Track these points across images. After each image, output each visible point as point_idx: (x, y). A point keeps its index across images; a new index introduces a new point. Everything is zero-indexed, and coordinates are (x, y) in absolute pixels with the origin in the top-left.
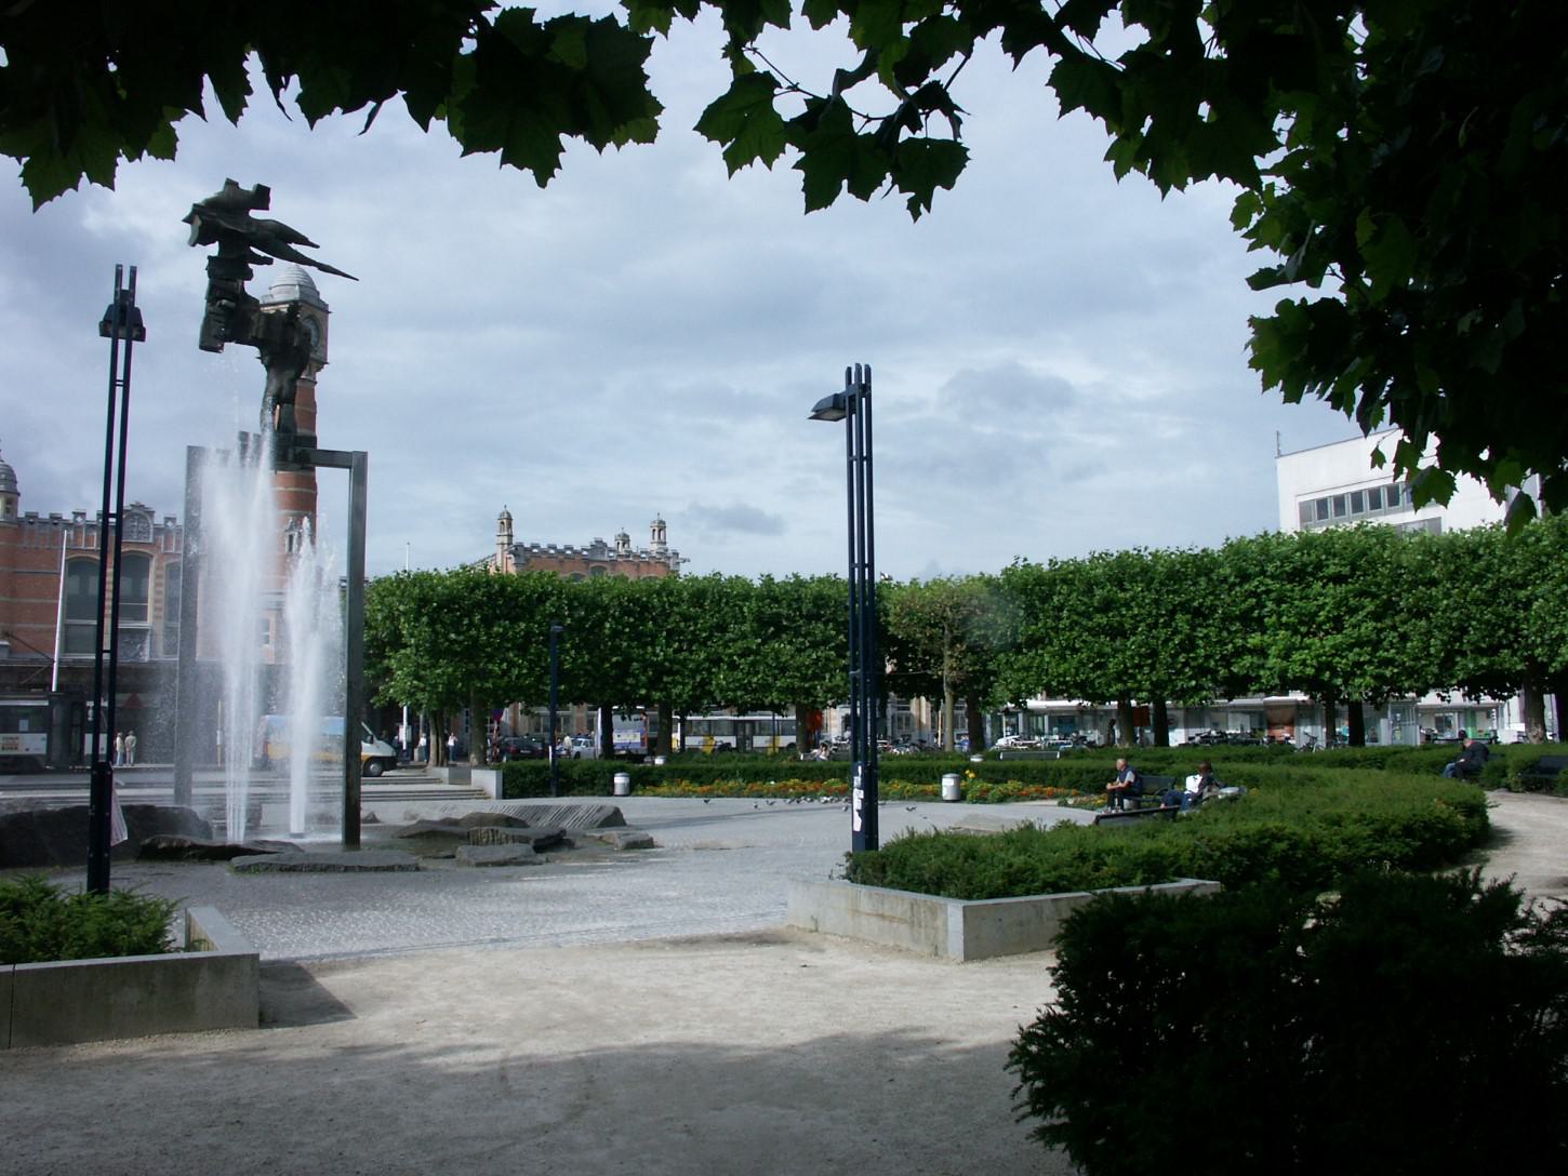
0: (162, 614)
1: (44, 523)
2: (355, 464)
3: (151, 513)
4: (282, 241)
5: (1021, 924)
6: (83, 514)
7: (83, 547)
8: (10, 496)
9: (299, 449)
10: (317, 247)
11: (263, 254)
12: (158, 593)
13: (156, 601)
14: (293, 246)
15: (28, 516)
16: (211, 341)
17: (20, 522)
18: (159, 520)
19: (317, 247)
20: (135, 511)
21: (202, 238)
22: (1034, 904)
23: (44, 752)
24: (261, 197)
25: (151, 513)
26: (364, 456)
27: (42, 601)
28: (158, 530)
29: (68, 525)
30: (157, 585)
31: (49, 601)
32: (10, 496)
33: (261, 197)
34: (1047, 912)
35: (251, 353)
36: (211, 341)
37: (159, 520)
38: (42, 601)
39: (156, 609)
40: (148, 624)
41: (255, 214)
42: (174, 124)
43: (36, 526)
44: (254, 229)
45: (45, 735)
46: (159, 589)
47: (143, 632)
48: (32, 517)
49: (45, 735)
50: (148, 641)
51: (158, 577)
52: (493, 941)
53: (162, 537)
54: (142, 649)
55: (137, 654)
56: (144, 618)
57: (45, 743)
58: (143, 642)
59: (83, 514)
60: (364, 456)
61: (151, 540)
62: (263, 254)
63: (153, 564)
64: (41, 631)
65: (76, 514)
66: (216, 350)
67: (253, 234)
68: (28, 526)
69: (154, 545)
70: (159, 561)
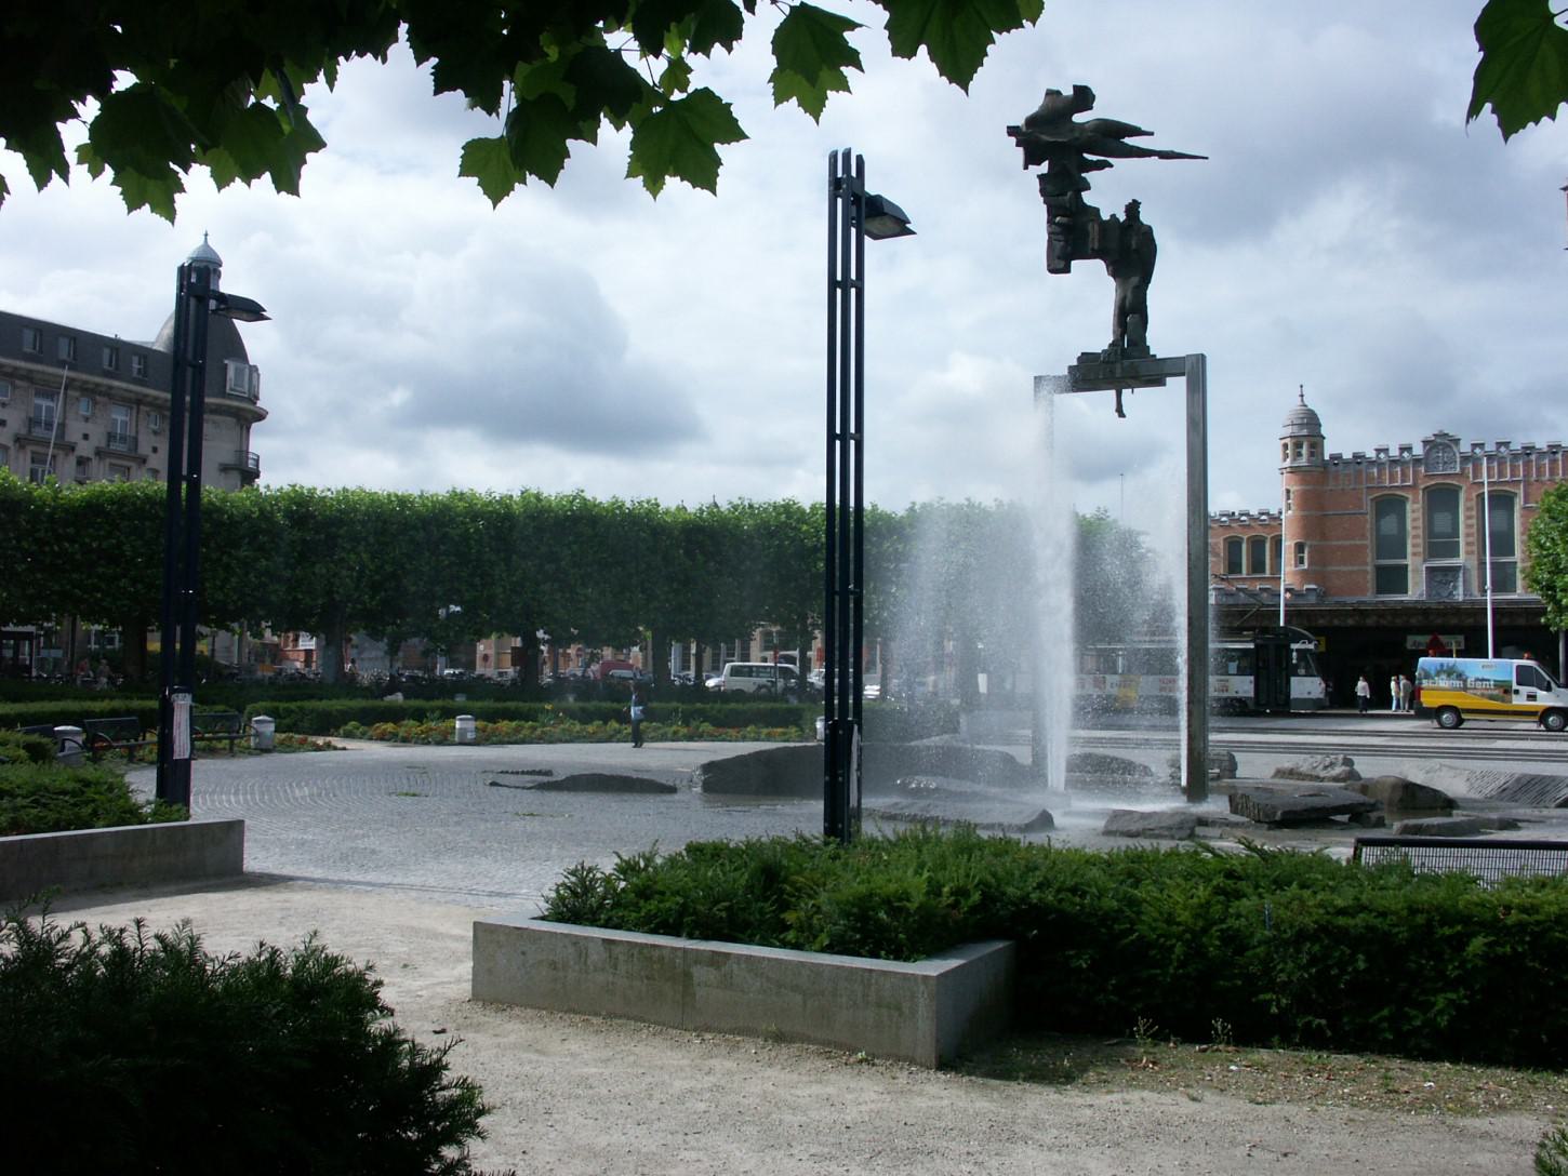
0: (1421, 550)
1: (1347, 463)
2: (1193, 370)
3: (1457, 441)
4: (1114, 139)
5: (553, 965)
6: (1386, 450)
7: (1387, 484)
8: (1313, 439)
9: (1126, 362)
10: (1152, 134)
11: (1095, 158)
12: (1469, 526)
13: (1468, 535)
14: (1127, 140)
15: (1333, 457)
16: (1059, 262)
17: (1325, 464)
18: (1465, 448)
19: (1152, 134)
20: (1439, 440)
21: (1031, 159)
22: (576, 941)
23: (1252, 694)
24: (1083, 97)
25: (1457, 441)
26: (1201, 359)
27: (1352, 542)
28: (1465, 459)
29: (1372, 463)
30: (1468, 518)
31: (1358, 542)
32: (1313, 439)
33: (1083, 97)
34: (594, 957)
35: (1099, 265)
36: (1059, 262)
37: (1465, 448)
38: (1352, 542)
39: (1468, 544)
40: (1460, 561)
41: (1078, 118)
42: (59, 125)
43: (1341, 467)
44: (1077, 134)
45: (1252, 678)
46: (1470, 522)
47: (1455, 570)
48: (1336, 458)
49: (1252, 678)
50: (1461, 575)
51: (1468, 509)
52: (491, 894)
53: (1470, 466)
54: (1455, 588)
55: (1451, 593)
56: (1457, 555)
57: (1252, 686)
58: (1456, 579)
59: (1386, 450)
60: (1201, 359)
61: (1458, 470)
62: (1095, 158)
63: (1462, 496)
64: (1351, 572)
65: (1379, 451)
66: (1067, 270)
67: (1077, 139)
68: (1334, 468)
69: (1462, 474)
70: (1468, 492)
